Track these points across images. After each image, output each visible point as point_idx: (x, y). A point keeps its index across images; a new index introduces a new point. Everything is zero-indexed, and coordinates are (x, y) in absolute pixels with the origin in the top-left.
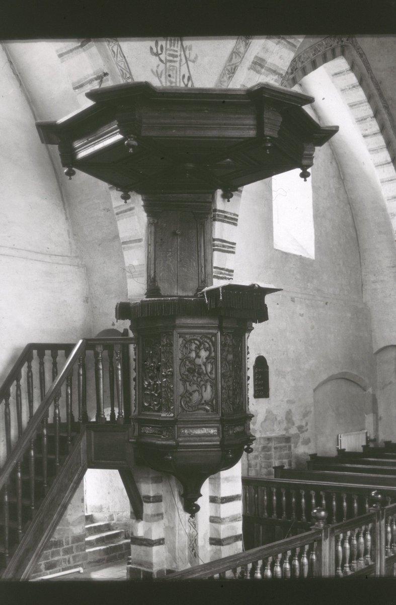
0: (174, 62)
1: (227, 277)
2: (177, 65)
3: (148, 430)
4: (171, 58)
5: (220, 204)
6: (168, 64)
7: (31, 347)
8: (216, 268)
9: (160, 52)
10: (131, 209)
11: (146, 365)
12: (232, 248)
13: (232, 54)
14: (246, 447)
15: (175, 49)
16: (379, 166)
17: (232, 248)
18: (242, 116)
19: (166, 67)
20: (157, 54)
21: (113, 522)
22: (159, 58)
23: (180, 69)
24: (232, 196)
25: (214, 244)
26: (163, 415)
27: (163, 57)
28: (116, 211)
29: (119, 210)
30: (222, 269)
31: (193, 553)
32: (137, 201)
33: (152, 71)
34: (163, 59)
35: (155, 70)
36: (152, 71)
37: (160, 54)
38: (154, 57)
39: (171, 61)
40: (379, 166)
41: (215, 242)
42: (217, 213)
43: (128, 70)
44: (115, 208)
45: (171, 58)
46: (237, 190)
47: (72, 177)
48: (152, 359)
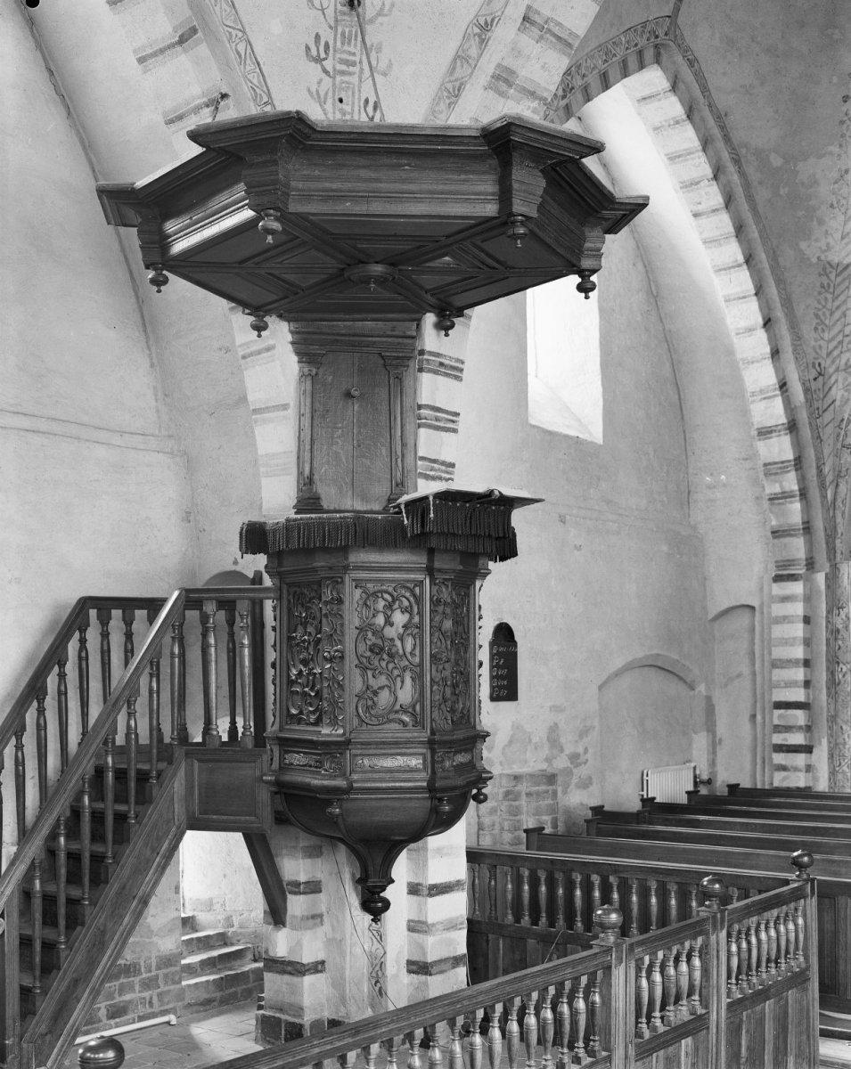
0: (350, 74)
1: (444, 475)
2: (355, 79)
3: (297, 759)
4: (344, 67)
5: (431, 338)
6: (338, 78)
7: (85, 603)
8: (422, 458)
9: (323, 55)
10: (268, 349)
11: (295, 638)
12: (453, 422)
13: (455, 60)
14: (474, 791)
15: (352, 49)
16: (720, 270)
17: (453, 422)
18: (471, 176)
19: (334, 84)
20: (318, 60)
21: (231, 930)
22: (322, 66)
23: (360, 87)
24: (452, 326)
25: (419, 415)
26: (325, 731)
27: (328, 64)
28: (241, 353)
29: (248, 351)
30: (434, 461)
31: (377, 989)
32: (280, 332)
33: (309, 90)
34: (329, 68)
35: (314, 90)
36: (309, 90)
37: (325, 59)
38: (313, 63)
39: (343, 73)
40: (720, 270)
41: (422, 411)
42: (425, 357)
43: (265, 89)
44: (240, 346)
45: (344, 67)
46: (462, 315)
47: (162, 288)
48: (305, 628)
